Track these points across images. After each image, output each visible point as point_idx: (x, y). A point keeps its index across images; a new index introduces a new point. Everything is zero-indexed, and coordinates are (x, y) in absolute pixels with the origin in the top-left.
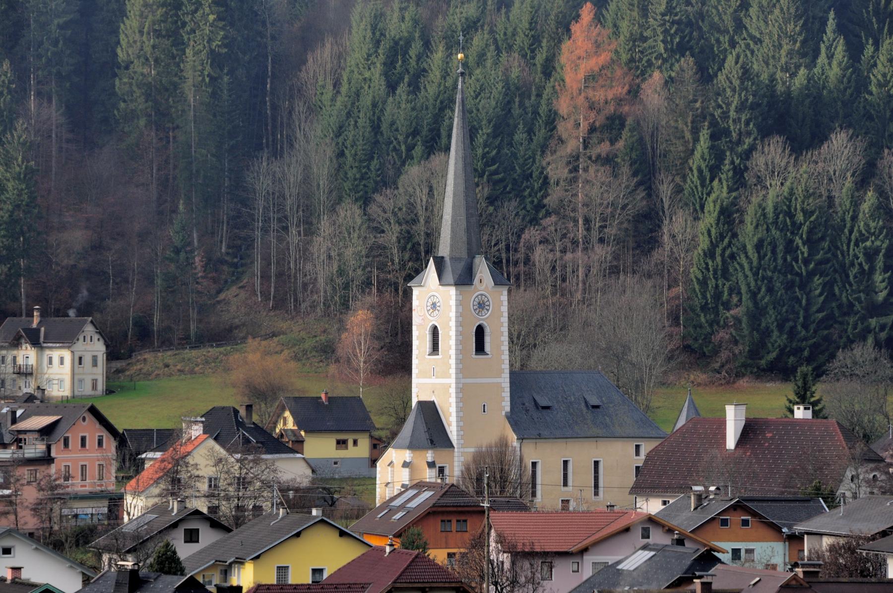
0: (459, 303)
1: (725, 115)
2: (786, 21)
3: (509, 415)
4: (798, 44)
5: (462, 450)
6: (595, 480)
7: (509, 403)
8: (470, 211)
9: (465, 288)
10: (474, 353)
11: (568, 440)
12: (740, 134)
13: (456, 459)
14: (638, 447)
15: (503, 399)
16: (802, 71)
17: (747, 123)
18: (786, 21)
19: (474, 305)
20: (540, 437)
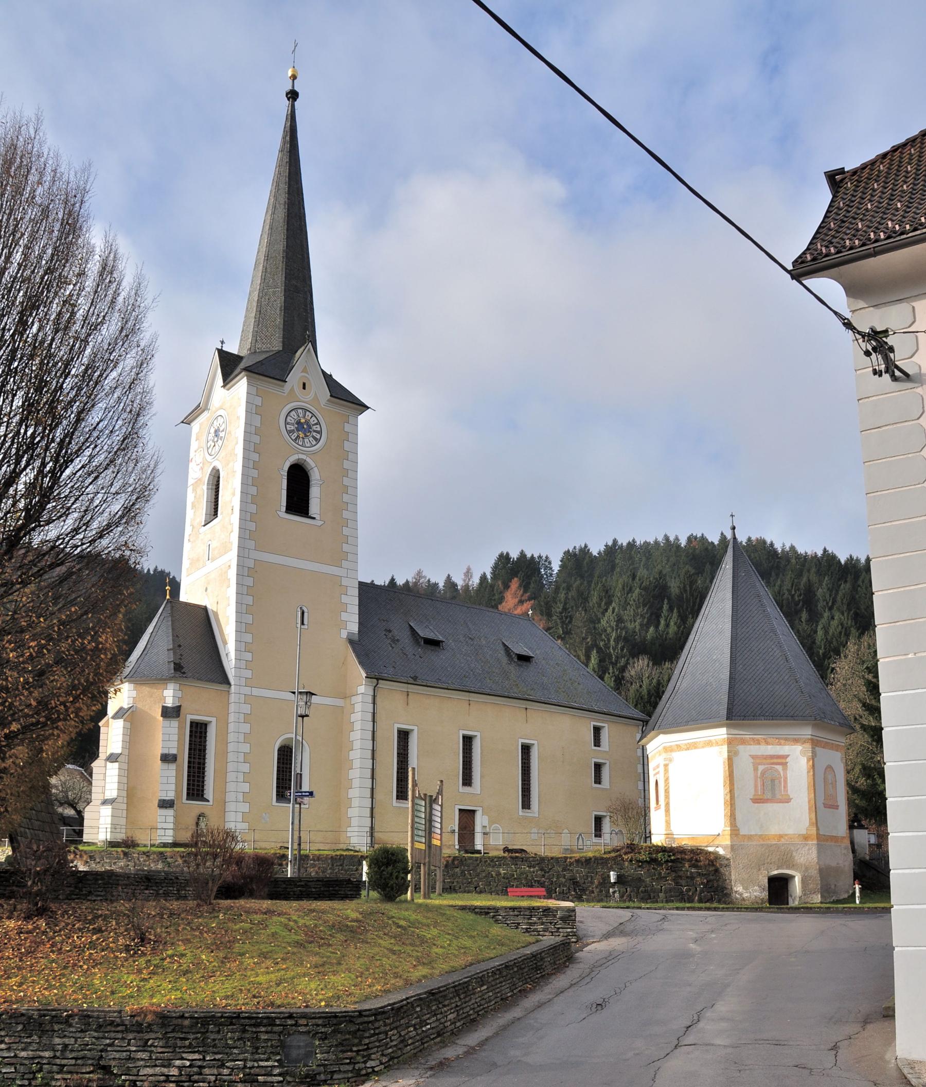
0: (252, 410)
1: (607, 646)
2: (638, 608)
3: (356, 638)
4: (646, 620)
5: (247, 690)
6: (523, 796)
7: (356, 618)
8: (294, 282)
9: (269, 386)
10: (284, 509)
11: (474, 697)
12: (617, 657)
13: (232, 708)
14: (597, 730)
15: (344, 608)
16: (652, 629)
17: (622, 650)
18: (638, 608)
19: (286, 423)
20: (415, 680)
